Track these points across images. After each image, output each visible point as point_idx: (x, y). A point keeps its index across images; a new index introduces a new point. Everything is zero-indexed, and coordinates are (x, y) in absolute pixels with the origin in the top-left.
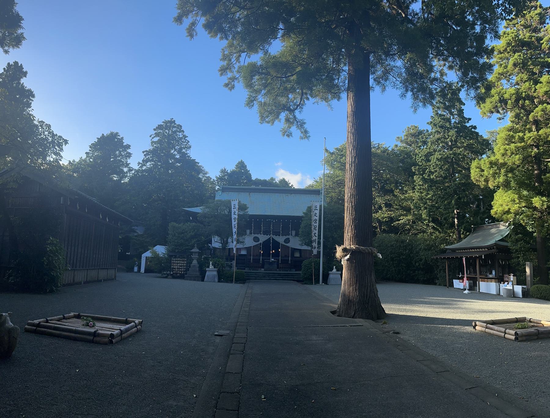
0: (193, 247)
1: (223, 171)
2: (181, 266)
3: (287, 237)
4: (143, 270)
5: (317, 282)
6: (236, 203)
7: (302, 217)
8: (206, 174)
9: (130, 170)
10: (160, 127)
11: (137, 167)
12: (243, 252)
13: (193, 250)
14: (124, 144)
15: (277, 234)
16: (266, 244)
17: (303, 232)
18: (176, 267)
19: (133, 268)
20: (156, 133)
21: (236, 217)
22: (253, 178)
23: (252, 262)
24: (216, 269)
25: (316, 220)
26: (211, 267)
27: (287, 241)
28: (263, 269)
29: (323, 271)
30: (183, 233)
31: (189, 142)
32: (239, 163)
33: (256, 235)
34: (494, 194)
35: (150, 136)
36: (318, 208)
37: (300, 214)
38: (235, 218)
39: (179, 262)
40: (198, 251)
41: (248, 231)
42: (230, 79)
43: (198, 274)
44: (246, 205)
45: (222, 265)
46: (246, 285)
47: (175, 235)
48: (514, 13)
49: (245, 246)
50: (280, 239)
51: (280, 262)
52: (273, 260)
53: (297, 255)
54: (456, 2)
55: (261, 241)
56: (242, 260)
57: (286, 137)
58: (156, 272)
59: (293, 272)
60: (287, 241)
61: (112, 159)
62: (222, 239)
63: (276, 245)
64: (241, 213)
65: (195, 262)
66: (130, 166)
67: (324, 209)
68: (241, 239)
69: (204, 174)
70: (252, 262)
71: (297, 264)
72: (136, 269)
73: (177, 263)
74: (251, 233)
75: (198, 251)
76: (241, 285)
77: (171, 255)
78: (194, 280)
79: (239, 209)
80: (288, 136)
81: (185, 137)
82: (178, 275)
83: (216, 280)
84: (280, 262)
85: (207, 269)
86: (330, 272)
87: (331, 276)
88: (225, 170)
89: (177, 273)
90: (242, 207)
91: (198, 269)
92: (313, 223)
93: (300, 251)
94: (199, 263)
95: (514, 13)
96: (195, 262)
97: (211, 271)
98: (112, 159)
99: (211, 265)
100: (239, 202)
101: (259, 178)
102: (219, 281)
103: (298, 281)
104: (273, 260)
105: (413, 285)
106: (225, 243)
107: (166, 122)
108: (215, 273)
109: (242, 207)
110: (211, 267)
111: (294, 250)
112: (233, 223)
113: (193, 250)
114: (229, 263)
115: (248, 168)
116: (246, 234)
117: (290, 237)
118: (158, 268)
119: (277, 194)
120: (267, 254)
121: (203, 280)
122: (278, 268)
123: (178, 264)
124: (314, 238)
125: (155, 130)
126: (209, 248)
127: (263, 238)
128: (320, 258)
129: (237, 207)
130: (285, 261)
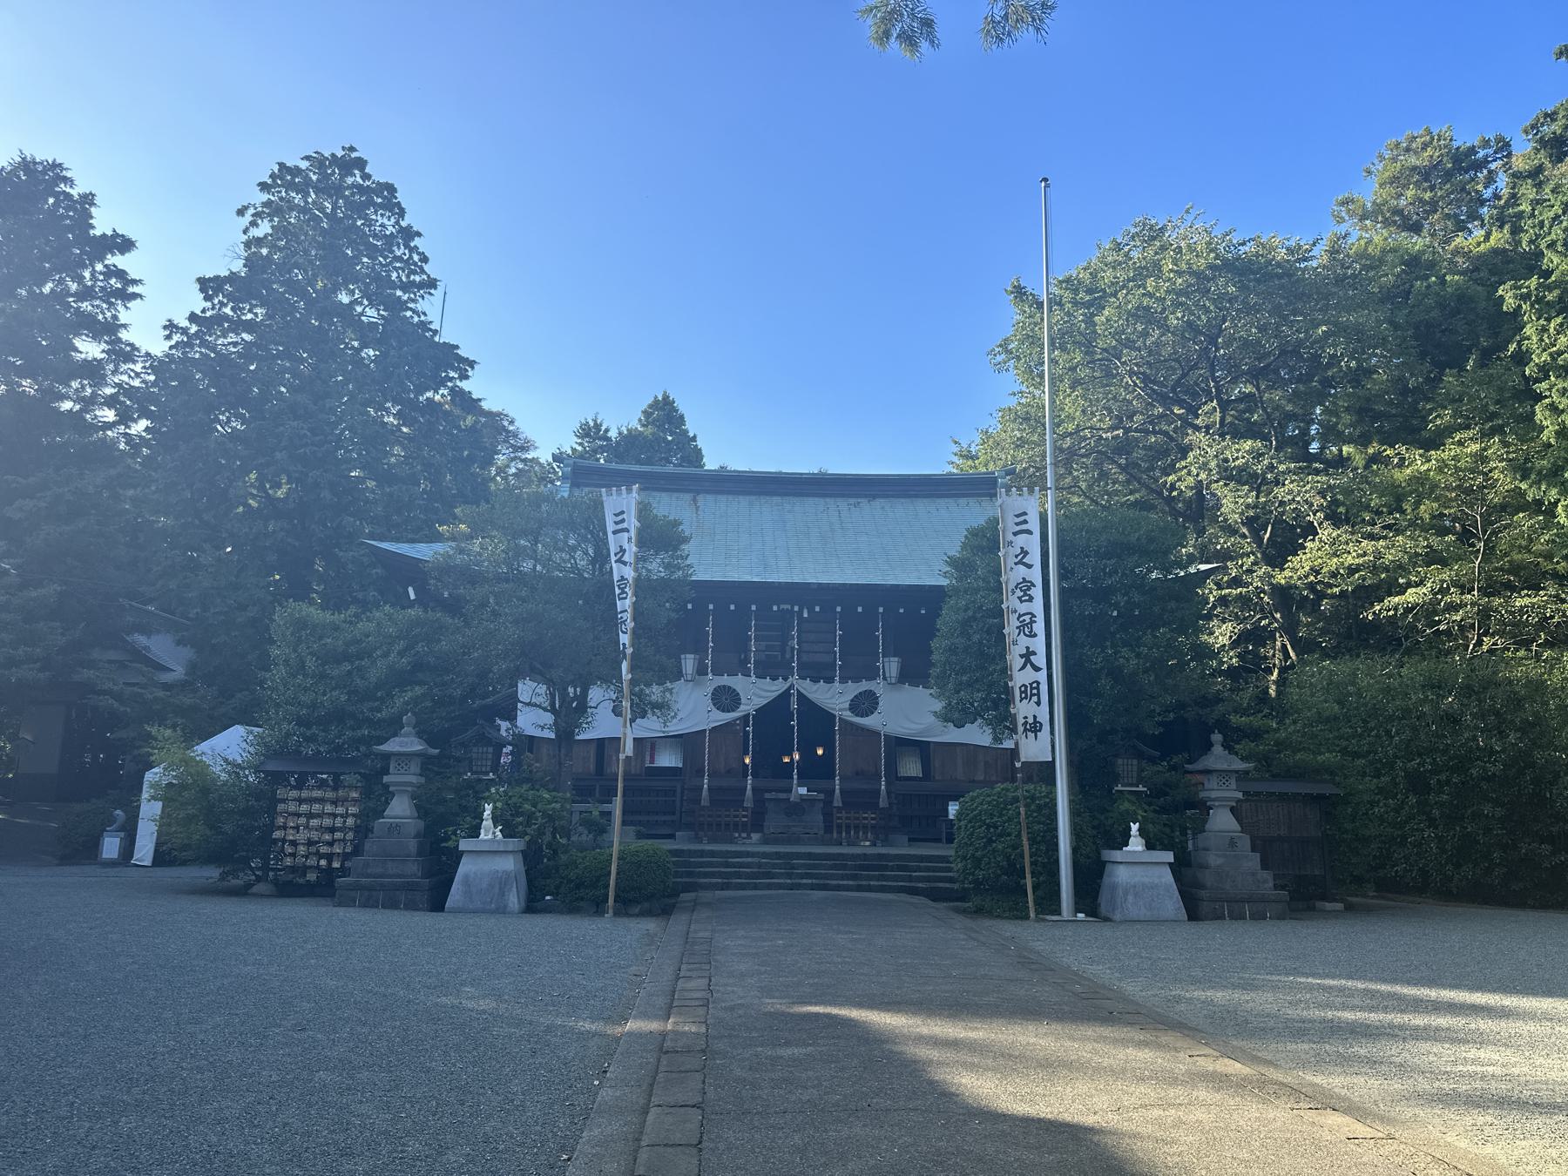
0: (393, 727)
2: (332, 830)
3: (865, 686)
4: (144, 850)
5: (1049, 902)
7: (931, 597)
8: (524, 449)
9: (123, 354)
10: (285, 175)
11: (157, 346)
12: (667, 759)
13: (392, 746)
14: (98, 232)
16: (774, 712)
17: (952, 650)
19: (94, 845)
20: (268, 204)
22: (711, 463)
23: (705, 801)
24: (516, 844)
25: (1027, 585)
26: (489, 831)
27: (867, 703)
28: (755, 836)
29: (1075, 850)
30: (346, 657)
31: (425, 259)
32: (655, 405)
33: (725, 680)
35: (241, 212)
36: (1034, 525)
37: (932, 574)
39: (316, 807)
40: (417, 746)
43: (413, 869)
45: (551, 819)
46: (678, 923)
47: (302, 665)
49: (675, 728)
50: (835, 697)
51: (837, 802)
52: (803, 791)
53: (911, 767)
56: (657, 796)
58: (184, 863)
59: (902, 848)
63: (818, 721)
64: (656, 568)
65: (400, 808)
66: (124, 335)
67: (1060, 531)
68: (655, 693)
69: (516, 449)
70: (705, 801)
71: (918, 812)
72: (111, 847)
73: (310, 816)
74: (701, 671)
75: (417, 746)
76: (650, 925)
77: (280, 769)
78: (392, 904)
80: (909, 39)
81: (409, 234)
82: (312, 876)
83: (514, 900)
84: (837, 802)
85: (464, 845)
87: (1121, 875)
89: (304, 870)
91: (412, 845)
92: (1011, 602)
93: (923, 749)
94: (422, 810)
96: (400, 808)
97: (489, 854)
99: (487, 823)
102: (532, 905)
103: (936, 896)
104: (803, 791)
105: (1532, 915)
106: (570, 713)
107: (318, 162)
108: (510, 864)
110: (489, 831)
111: (900, 744)
113: (392, 746)
114: (595, 810)
115: (691, 427)
117: (878, 686)
118: (232, 846)
119: (811, 501)
120: (771, 769)
121: (438, 905)
122: (828, 829)
123: (311, 821)
124: (1021, 678)
125: (264, 187)
127: (755, 693)
128: (1054, 784)
129: (633, 523)
130: (859, 799)
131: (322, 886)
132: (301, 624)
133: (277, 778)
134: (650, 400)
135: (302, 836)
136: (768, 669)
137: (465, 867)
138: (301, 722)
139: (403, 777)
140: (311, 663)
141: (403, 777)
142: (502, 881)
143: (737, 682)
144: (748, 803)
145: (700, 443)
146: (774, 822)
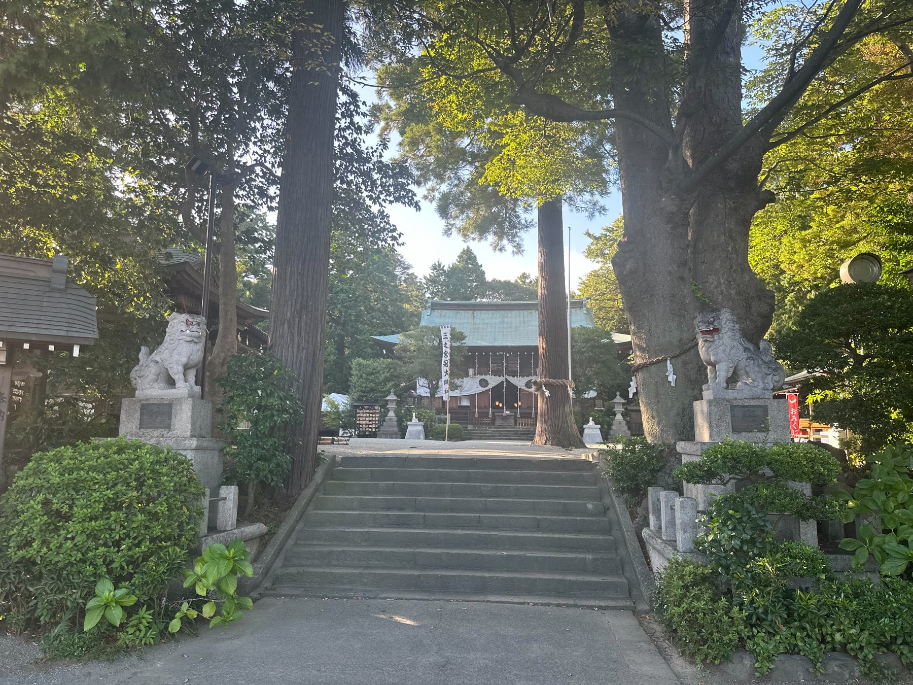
1: (437, 267)
6: (448, 330)
8: (408, 268)
12: (465, 403)
13: (389, 398)
15: (514, 375)
16: (497, 389)
18: (364, 422)
21: (448, 350)
22: (489, 278)
26: (415, 420)
32: (464, 252)
33: (483, 377)
34: (133, 374)
42: (429, 190)
43: (396, 429)
44: (462, 333)
47: (361, 376)
50: (520, 382)
51: (519, 416)
55: (490, 387)
56: (460, 414)
57: (497, 252)
62: (430, 382)
63: (512, 388)
65: (391, 414)
68: (457, 382)
74: (475, 374)
78: (392, 438)
79: (452, 339)
80: (501, 250)
83: (422, 436)
84: (519, 416)
86: (585, 426)
88: (440, 265)
90: (457, 336)
91: (395, 423)
96: (391, 414)
100: (453, 329)
101: (498, 278)
106: (434, 389)
108: (421, 428)
109: (457, 336)
110: (415, 420)
113: (389, 398)
114: (442, 416)
115: (480, 261)
119: (515, 312)
121: (403, 437)
126: (411, 396)
127: (493, 381)
129: (449, 336)
131: (373, 435)
132: (360, 365)
133: (356, 407)
134: (461, 250)
135: (364, 422)
136: (497, 373)
137: (409, 429)
138: (363, 392)
139: (392, 406)
140: (364, 376)
141: (392, 406)
142: (419, 432)
143: (487, 378)
144: (490, 416)
145: (483, 268)
146: (498, 422)
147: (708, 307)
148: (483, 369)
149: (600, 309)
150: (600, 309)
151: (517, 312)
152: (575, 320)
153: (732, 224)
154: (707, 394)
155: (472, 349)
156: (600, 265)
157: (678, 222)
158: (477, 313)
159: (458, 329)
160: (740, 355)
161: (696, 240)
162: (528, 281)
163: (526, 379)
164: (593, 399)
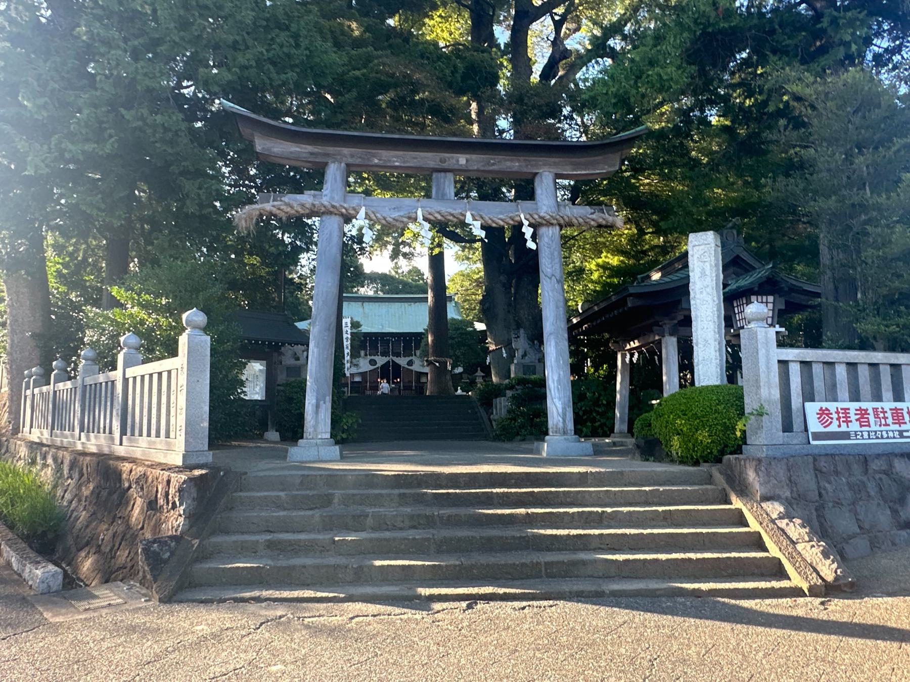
3: (410, 358)
12: (357, 379)
15: (398, 355)
16: (385, 367)
21: (349, 336)
27: (410, 363)
33: (373, 357)
38: (347, 338)
41: (362, 353)
48: (731, 92)
49: (360, 371)
50: (402, 361)
54: (268, 3)
55: (379, 365)
60: (410, 363)
61: (13, 167)
63: (397, 366)
74: (366, 355)
90: (355, 325)
95: (731, 92)
98: (13, 167)
112: (345, 343)
116: (360, 356)
117: (413, 358)
127: (381, 361)
129: (349, 325)
136: (384, 354)
147: (518, 326)
148: (374, 351)
149: (465, 301)
150: (465, 301)
151: (399, 304)
152: (452, 313)
153: (530, 287)
154: (515, 361)
155: (367, 335)
156: (466, 266)
157: (507, 287)
158: (366, 304)
159: (355, 319)
160: (527, 346)
161: (515, 293)
162: (400, 271)
163: (408, 359)
164: (460, 374)
